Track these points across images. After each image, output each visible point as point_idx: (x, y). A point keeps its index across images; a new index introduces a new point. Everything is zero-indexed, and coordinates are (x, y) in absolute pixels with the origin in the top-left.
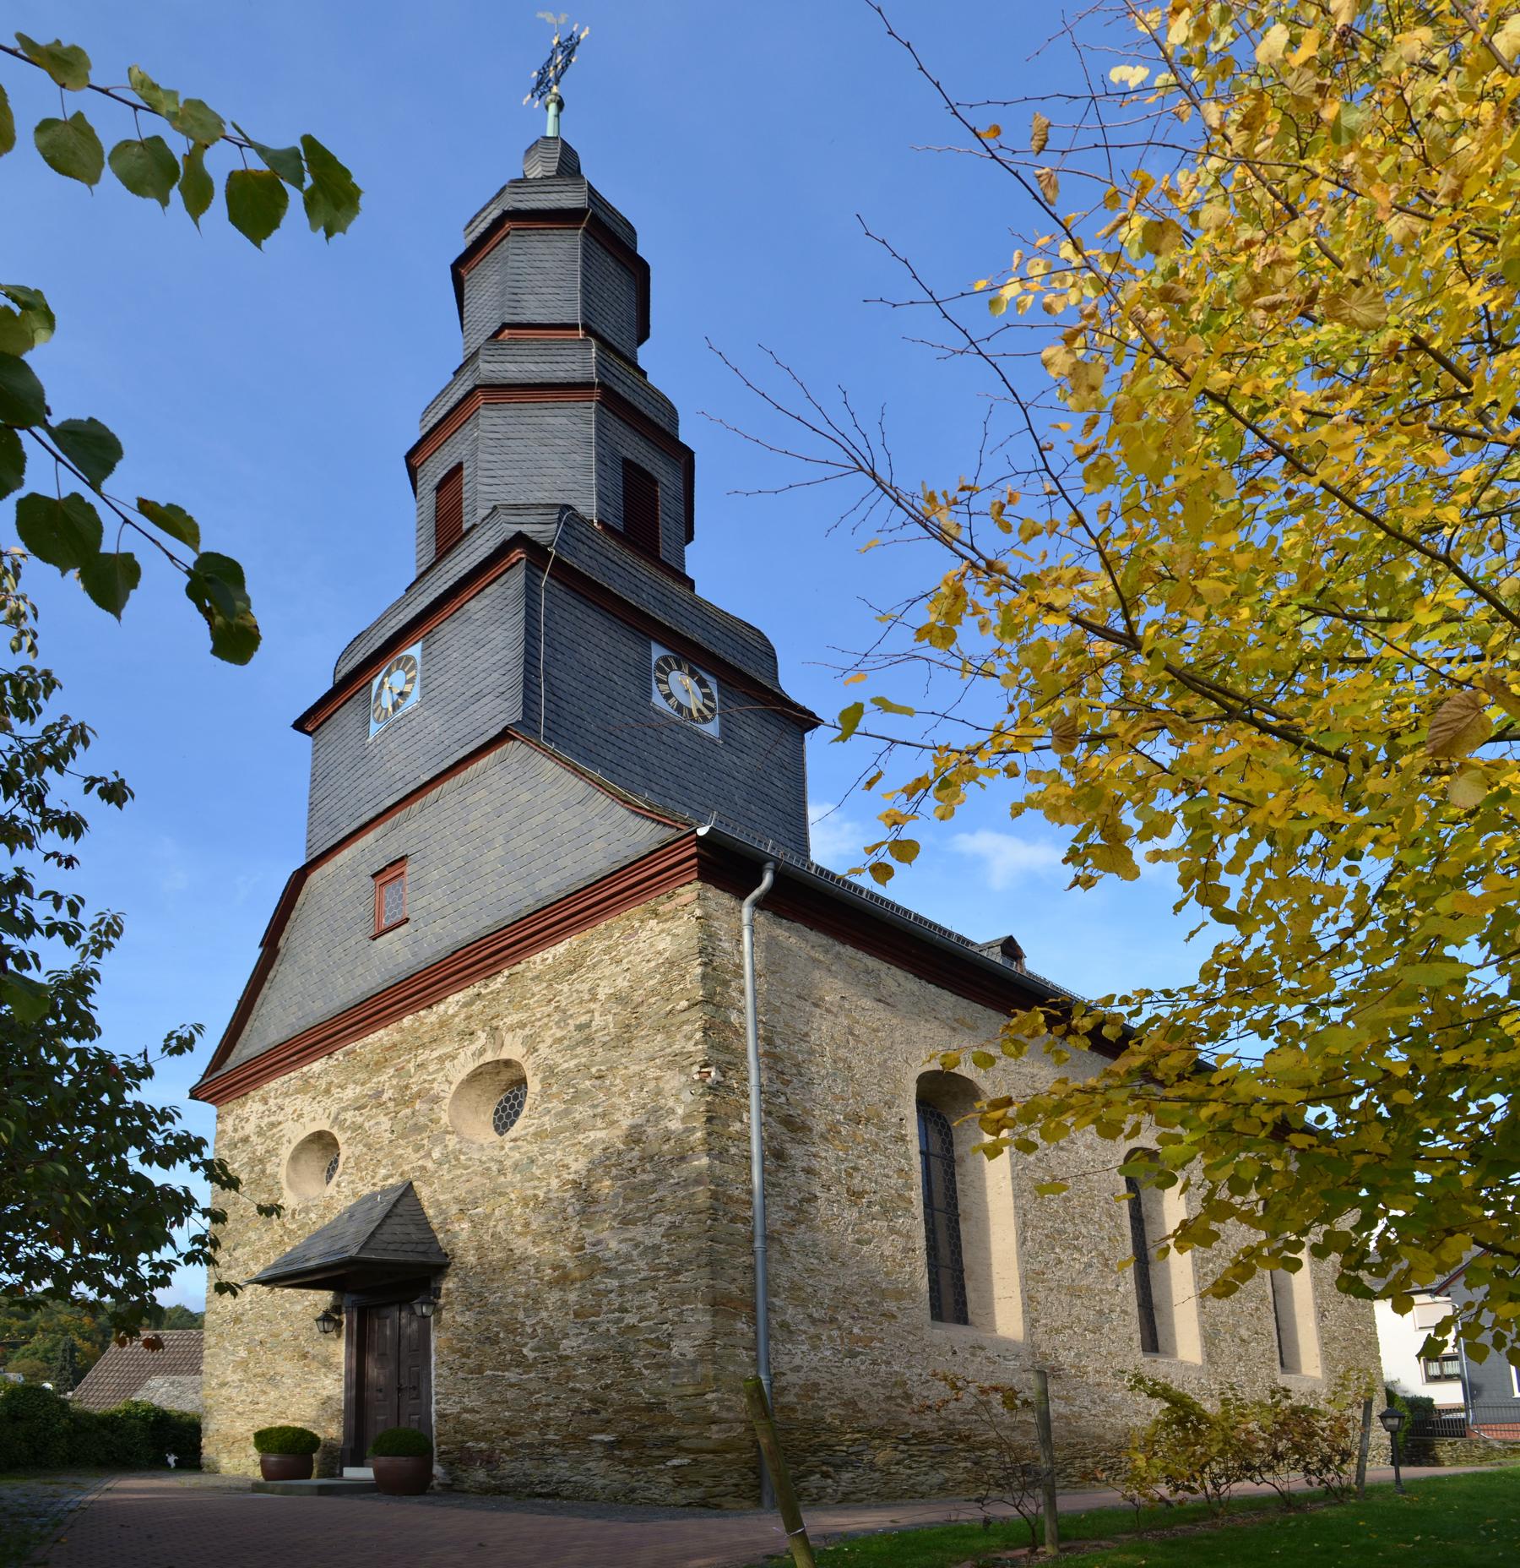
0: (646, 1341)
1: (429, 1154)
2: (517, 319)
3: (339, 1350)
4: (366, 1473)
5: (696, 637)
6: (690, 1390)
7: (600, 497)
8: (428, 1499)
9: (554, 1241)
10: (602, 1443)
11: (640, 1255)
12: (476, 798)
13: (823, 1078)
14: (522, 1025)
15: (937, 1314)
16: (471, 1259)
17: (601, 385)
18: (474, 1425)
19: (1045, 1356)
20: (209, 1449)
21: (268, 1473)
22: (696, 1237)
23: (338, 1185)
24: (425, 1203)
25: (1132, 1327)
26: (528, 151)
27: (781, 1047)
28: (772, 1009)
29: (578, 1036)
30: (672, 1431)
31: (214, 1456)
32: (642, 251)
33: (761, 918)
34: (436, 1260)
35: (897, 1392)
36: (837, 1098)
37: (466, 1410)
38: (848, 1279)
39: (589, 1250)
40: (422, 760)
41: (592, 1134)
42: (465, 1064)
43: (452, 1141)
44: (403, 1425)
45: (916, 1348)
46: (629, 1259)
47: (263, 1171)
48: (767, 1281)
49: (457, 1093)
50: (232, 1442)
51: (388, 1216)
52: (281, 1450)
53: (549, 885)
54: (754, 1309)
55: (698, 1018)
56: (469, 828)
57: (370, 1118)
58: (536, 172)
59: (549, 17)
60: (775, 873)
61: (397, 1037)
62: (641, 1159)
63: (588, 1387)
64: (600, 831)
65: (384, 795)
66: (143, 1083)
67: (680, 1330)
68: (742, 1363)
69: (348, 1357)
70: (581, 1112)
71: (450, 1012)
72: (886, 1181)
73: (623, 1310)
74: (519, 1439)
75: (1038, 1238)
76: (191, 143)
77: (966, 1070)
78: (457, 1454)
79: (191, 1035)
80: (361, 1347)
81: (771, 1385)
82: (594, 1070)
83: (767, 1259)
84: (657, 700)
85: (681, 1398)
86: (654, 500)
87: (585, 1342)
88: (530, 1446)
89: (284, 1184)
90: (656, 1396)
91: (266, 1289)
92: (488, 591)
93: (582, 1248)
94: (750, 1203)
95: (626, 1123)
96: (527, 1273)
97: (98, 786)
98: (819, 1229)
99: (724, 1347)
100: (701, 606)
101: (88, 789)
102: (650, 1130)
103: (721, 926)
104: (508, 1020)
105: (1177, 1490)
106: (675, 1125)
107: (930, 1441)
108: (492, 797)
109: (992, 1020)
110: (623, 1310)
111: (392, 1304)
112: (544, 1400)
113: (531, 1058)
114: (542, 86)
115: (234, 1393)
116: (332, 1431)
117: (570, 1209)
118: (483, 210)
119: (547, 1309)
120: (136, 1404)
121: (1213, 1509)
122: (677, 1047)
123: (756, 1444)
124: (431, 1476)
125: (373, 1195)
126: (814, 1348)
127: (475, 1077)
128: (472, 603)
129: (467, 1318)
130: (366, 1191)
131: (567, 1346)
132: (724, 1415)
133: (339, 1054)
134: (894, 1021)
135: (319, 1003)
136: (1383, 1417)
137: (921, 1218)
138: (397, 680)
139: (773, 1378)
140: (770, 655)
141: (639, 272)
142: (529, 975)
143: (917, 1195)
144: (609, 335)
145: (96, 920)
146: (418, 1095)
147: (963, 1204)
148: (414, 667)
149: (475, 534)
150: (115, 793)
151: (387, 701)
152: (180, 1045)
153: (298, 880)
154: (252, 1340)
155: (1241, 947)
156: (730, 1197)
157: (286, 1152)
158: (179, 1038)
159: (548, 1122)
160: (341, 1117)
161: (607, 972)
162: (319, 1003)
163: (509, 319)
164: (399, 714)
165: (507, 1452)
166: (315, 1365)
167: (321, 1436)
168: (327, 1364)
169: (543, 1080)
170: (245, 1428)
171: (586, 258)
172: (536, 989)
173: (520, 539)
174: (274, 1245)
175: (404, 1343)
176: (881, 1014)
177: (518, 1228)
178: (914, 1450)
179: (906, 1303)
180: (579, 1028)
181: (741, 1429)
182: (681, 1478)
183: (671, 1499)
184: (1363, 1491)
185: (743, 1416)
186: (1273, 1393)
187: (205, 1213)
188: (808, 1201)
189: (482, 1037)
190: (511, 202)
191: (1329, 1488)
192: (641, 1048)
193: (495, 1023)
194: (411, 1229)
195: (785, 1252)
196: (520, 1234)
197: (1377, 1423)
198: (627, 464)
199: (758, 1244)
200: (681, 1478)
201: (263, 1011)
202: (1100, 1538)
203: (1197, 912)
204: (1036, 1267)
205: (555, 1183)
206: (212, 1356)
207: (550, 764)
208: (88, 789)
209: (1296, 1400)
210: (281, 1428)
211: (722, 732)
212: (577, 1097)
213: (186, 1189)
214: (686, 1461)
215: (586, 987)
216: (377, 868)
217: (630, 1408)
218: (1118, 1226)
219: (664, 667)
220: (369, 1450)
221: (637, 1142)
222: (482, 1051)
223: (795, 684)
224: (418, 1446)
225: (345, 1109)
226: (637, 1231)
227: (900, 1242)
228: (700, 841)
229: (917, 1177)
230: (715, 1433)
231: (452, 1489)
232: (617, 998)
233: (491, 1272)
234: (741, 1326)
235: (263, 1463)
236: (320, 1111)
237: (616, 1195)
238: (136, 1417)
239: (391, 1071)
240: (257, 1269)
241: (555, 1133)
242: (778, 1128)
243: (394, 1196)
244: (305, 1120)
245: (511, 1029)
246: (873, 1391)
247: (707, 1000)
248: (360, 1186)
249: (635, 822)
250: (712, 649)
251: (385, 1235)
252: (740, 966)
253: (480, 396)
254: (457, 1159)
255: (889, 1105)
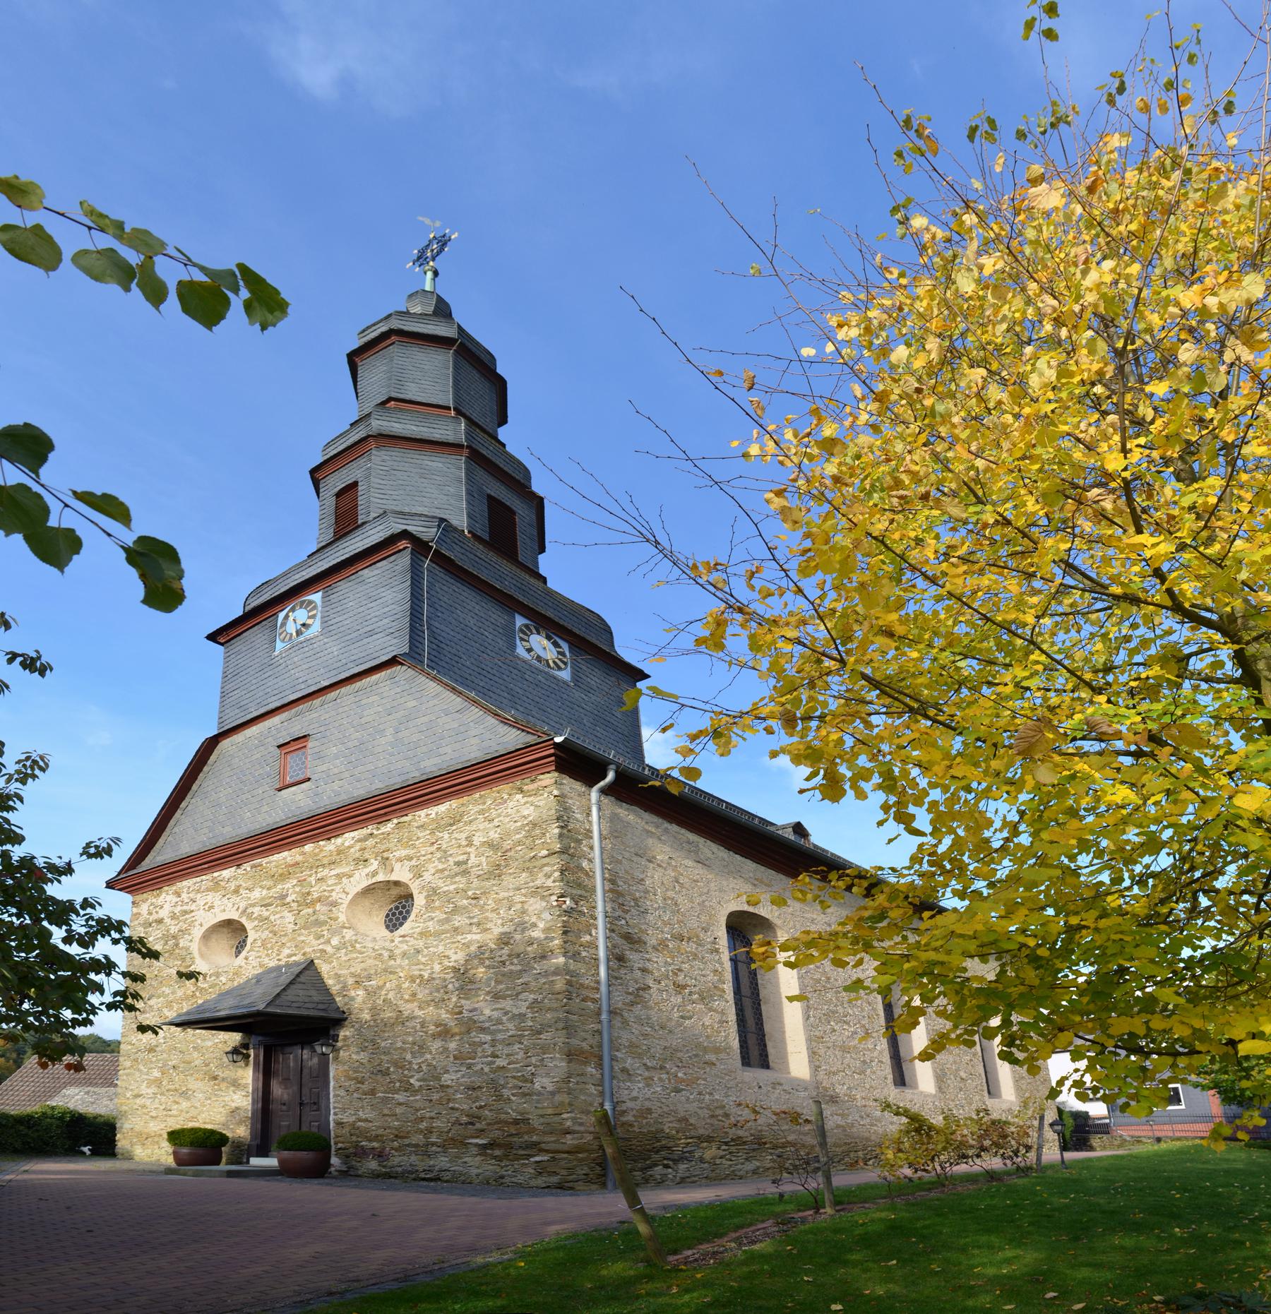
0: (514, 1077)
1: (328, 942)
2: (401, 396)
3: (247, 1075)
4: (271, 1162)
5: (550, 614)
6: (550, 1111)
7: (469, 516)
8: (326, 1181)
9: (437, 1006)
10: (476, 1145)
11: (509, 1020)
12: (370, 700)
13: (656, 909)
14: (410, 859)
15: (746, 1061)
16: (366, 1016)
17: (468, 447)
18: (368, 1130)
19: (826, 1089)
20: (122, 1142)
21: (180, 1161)
22: (556, 1010)
23: (246, 958)
24: (325, 976)
25: (887, 1071)
26: (410, 296)
27: (622, 887)
28: (614, 860)
29: (456, 869)
30: (535, 1138)
31: (128, 1147)
32: (500, 370)
33: (606, 800)
34: (337, 1016)
35: (719, 1112)
36: (665, 923)
37: (360, 1120)
38: (675, 1041)
39: (466, 1014)
40: (322, 671)
41: (469, 937)
42: (360, 880)
43: (348, 934)
44: (304, 1129)
45: (732, 1084)
46: (499, 1022)
47: (177, 945)
48: (611, 1041)
49: (353, 902)
50: (145, 1138)
51: (291, 983)
52: (192, 1144)
53: (432, 765)
54: (601, 1058)
55: (555, 864)
56: (363, 721)
57: (275, 913)
58: (417, 309)
59: (427, 221)
60: (616, 772)
61: (299, 858)
62: (509, 956)
63: (465, 1107)
64: (473, 733)
65: (287, 692)
66: (63, 878)
67: (541, 1071)
68: (591, 1095)
69: (255, 1080)
70: (459, 920)
71: (347, 844)
72: (703, 979)
73: (495, 1056)
74: (407, 1141)
75: (818, 1015)
76: (142, 257)
77: (764, 911)
78: (351, 1150)
79: (109, 846)
80: (267, 1072)
81: (614, 1109)
82: (470, 893)
83: (610, 1026)
84: (520, 651)
85: (542, 1116)
86: (514, 524)
87: (463, 1076)
88: (416, 1146)
89: (196, 954)
90: (522, 1114)
91: (179, 1029)
92: (379, 565)
93: (461, 1013)
94: (598, 989)
95: (497, 931)
96: (414, 1027)
97: (20, 659)
98: (651, 1008)
99: (577, 1083)
100: (551, 594)
101: (10, 661)
102: (518, 937)
103: (574, 803)
104: (397, 854)
105: (916, 1171)
106: (537, 934)
107: (745, 1143)
108: (384, 701)
109: (781, 882)
110: (495, 1056)
111: (296, 1044)
112: (428, 1115)
113: (418, 882)
114: (421, 259)
115: (148, 1103)
116: (241, 1132)
117: (450, 986)
118: (374, 325)
119: (431, 1053)
120: (53, 1108)
121: (942, 1182)
122: (538, 883)
123: (601, 1147)
124: (329, 1165)
125: (278, 968)
126: (648, 1085)
127: (368, 891)
128: (366, 571)
129: (363, 1057)
130: (272, 964)
131: (447, 1079)
132: (577, 1128)
133: (247, 866)
134: (710, 876)
135: (228, 829)
136: (1051, 1125)
137: (732, 1002)
138: (301, 615)
139: (615, 1105)
140: (607, 631)
141: (500, 385)
142: (416, 824)
143: (728, 987)
144: (474, 417)
145: (23, 757)
146: (319, 900)
147: (763, 993)
148: (315, 608)
149: (367, 527)
150: (33, 664)
151: (291, 628)
152: (97, 852)
153: (209, 746)
154: (164, 1065)
155: (936, 846)
156: (582, 985)
157: (198, 932)
158: (97, 847)
159: (431, 926)
160: (249, 911)
161: (481, 827)
162: (228, 829)
163: (394, 395)
164: (302, 638)
165: (396, 1150)
166: (223, 1086)
167: (229, 1134)
168: (235, 1084)
169: (426, 897)
170: (160, 1128)
171: (456, 368)
172: (421, 835)
173: (405, 534)
174: (187, 998)
175: (305, 1071)
176: (699, 871)
177: (407, 997)
178: (733, 1149)
179: (722, 1056)
180: (458, 864)
181: (590, 1137)
182: (541, 1170)
183: (533, 1183)
184: (1040, 1168)
185: (592, 1129)
186: (978, 1112)
187: (125, 974)
188: (643, 989)
189: (374, 864)
190: (396, 324)
191: (1018, 1167)
192: (509, 881)
193: (385, 855)
194: (313, 993)
195: (625, 1023)
196: (408, 1001)
197: (1046, 1127)
198: (490, 498)
199: (604, 1016)
200: (541, 1170)
201: (176, 830)
202: (865, 1202)
203: (893, 827)
204: (817, 1033)
205: (437, 968)
206: (127, 1075)
207: (433, 684)
208: (10, 661)
209: (995, 1116)
210: (192, 1129)
211: (572, 677)
212: (456, 910)
213: (106, 957)
214: (546, 1158)
215: (463, 836)
216: (282, 741)
217: (500, 1122)
218: (874, 1010)
219: (526, 631)
220: (274, 1146)
221: (507, 944)
222: (375, 873)
223: (626, 650)
224: (321, 1146)
225: (253, 905)
226: (507, 1004)
227: (717, 1017)
228: (556, 745)
229: (728, 976)
230: (569, 1140)
231: (347, 1174)
232: (490, 845)
233: (380, 1026)
234: (590, 1070)
235: (175, 1153)
236: (230, 905)
237: (490, 979)
238: (52, 1117)
239: (295, 882)
240: (171, 1015)
241: (437, 934)
242: (620, 941)
243: (297, 970)
244: (216, 910)
245: (400, 860)
246: (700, 1112)
247: (563, 851)
248: (266, 960)
249: (503, 729)
250: (561, 622)
251: (290, 995)
252: (590, 831)
253: (372, 442)
254: (353, 946)
255: (705, 930)
